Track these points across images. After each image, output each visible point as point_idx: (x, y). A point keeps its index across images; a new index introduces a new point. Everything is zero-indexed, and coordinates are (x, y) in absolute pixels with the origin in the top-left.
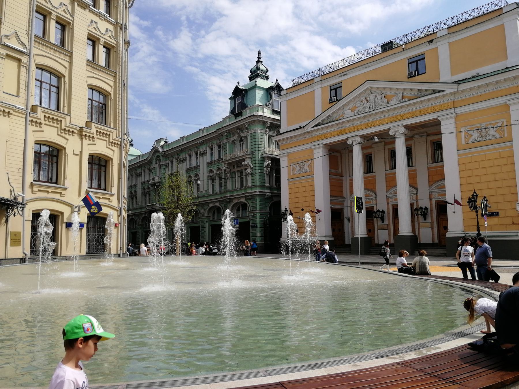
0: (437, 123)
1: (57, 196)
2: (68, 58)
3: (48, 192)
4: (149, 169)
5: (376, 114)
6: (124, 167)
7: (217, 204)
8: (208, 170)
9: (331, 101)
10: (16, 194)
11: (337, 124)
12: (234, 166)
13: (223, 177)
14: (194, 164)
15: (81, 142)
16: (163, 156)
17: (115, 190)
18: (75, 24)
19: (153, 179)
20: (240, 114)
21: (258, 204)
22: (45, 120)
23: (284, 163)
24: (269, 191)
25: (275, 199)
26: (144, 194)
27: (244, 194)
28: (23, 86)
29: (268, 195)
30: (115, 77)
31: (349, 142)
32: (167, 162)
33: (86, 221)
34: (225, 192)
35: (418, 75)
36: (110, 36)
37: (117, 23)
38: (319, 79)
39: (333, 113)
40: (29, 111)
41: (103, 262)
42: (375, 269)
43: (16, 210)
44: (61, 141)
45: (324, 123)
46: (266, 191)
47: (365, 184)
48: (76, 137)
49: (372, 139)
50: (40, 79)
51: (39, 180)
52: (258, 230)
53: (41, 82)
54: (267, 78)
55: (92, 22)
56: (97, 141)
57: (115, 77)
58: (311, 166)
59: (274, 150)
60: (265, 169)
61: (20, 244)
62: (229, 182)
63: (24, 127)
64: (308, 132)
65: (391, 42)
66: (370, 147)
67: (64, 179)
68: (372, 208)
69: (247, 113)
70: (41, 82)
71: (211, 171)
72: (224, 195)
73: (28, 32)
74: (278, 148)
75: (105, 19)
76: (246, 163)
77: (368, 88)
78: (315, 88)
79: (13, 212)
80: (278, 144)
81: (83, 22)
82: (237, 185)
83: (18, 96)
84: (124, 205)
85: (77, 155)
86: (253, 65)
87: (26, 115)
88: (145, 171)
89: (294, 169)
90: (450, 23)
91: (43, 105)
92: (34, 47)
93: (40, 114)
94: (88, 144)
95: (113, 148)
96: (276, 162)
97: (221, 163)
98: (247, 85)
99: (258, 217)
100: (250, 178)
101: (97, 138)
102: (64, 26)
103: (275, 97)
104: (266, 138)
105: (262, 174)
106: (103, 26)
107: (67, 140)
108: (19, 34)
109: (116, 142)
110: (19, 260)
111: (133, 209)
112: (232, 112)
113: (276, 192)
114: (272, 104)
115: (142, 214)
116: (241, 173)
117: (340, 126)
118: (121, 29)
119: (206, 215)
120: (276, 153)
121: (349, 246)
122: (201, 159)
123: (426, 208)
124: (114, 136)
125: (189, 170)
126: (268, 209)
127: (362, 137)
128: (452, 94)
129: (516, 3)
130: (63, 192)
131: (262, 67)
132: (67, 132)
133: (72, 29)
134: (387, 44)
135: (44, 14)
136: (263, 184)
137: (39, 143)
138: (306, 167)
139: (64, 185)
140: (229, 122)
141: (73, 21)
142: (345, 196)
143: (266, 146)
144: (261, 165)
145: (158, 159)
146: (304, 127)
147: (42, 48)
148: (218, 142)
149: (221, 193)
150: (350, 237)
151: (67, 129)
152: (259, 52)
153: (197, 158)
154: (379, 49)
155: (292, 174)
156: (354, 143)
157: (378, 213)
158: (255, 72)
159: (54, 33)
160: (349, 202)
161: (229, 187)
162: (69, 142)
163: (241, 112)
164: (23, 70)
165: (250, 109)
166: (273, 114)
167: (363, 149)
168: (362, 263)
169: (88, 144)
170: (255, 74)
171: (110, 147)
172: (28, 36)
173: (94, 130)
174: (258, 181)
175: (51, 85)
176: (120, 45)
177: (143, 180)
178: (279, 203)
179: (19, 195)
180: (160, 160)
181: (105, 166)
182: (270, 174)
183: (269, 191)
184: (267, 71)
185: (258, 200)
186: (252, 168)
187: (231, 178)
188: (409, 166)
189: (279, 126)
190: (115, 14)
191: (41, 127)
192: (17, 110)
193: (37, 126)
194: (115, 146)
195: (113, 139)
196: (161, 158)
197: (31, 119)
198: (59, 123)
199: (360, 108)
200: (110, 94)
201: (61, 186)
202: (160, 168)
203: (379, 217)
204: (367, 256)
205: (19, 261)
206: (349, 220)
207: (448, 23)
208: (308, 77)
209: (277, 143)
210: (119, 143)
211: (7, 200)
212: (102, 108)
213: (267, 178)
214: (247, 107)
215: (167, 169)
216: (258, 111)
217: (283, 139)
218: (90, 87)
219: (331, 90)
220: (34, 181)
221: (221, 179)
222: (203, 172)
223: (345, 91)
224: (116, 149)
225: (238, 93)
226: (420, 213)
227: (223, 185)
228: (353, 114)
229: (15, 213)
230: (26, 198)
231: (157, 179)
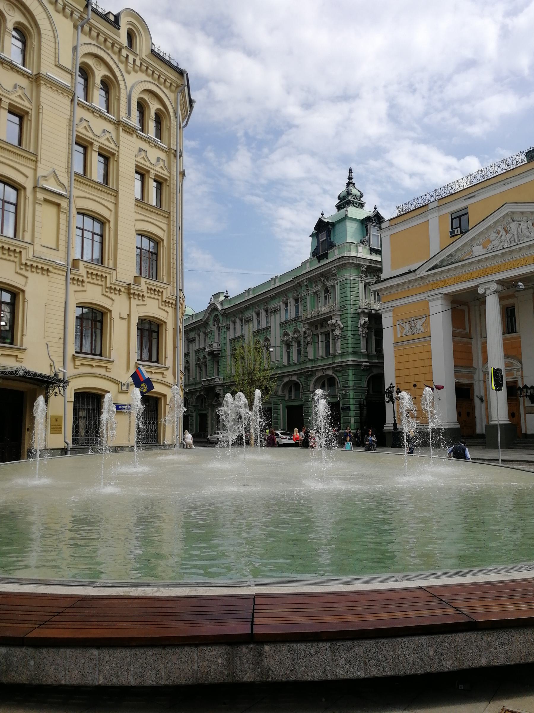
1: (102, 371)
2: (113, 197)
4: (204, 333)
5: (520, 249)
6: (180, 332)
7: (295, 378)
8: (282, 332)
9: (453, 234)
10: (57, 370)
11: (463, 266)
12: (316, 326)
13: (302, 342)
14: (263, 325)
15: (128, 302)
16: (224, 314)
17: (169, 362)
18: (120, 156)
19: (211, 345)
20: (325, 256)
21: (351, 378)
23: (387, 321)
24: (366, 360)
25: (375, 371)
26: (199, 366)
27: (330, 364)
28: (62, 237)
29: (364, 366)
30: (115, 196)
31: (480, 291)
32: (228, 323)
34: (305, 362)
36: (161, 167)
37: (170, 149)
38: (436, 204)
39: (456, 251)
40: (70, 267)
41: (162, 454)
42: (522, 469)
43: (57, 389)
44: (105, 303)
45: (444, 264)
46: (362, 360)
47: (504, 349)
48: (124, 297)
49: (516, 285)
50: (81, 227)
51: (81, 352)
52: (352, 413)
53: (83, 230)
54: (362, 205)
55: (140, 150)
56: (147, 301)
57: (168, 218)
58: (426, 325)
59: (372, 302)
60: (361, 329)
61: (61, 431)
62: (310, 348)
63: (64, 287)
64: (422, 278)
66: (512, 296)
67: (110, 350)
68: (516, 382)
69: (335, 254)
70: (83, 230)
71: (286, 334)
72: (303, 366)
73: (68, 169)
74: (379, 300)
75: (155, 146)
76: (333, 321)
77: (507, 214)
78: (430, 217)
79: (54, 391)
80: (378, 295)
82: (322, 352)
83: (57, 250)
84: (180, 381)
85: (125, 319)
86: (341, 189)
87: (67, 272)
88: (199, 336)
89: (402, 329)
91: (85, 259)
92: (74, 187)
93: (82, 270)
94: (137, 305)
95: (166, 309)
96: (375, 321)
97: (298, 323)
98: (335, 215)
99: (352, 396)
100: (339, 343)
101: (148, 297)
102: (107, 157)
103: (373, 230)
104: (362, 286)
105: (357, 337)
106: (153, 154)
108: (57, 172)
109: (171, 301)
110: (60, 451)
111: (189, 385)
112: (315, 253)
113: (376, 361)
114: (369, 241)
115: (196, 391)
116: (327, 335)
117: (466, 269)
118: (175, 156)
119: (280, 393)
120: (375, 307)
121: (482, 436)
122: (272, 319)
124: (167, 294)
125: (257, 333)
126: (365, 385)
127: (499, 282)
130: (20, 355)
131: (354, 191)
132: (112, 291)
133: (117, 161)
135: (84, 145)
136: (357, 350)
137: (80, 306)
138: (418, 326)
140: (310, 267)
141: (118, 152)
142: (475, 365)
143: (361, 299)
144: (354, 324)
145: (216, 319)
146: (415, 271)
147: (83, 188)
148: (295, 295)
149: (299, 363)
150: (484, 423)
151: (113, 287)
152: (350, 170)
153: (267, 317)
155: (399, 336)
156: (488, 292)
157: (525, 390)
158: (344, 198)
159: (97, 170)
160: (481, 375)
161: (311, 356)
162: (115, 302)
163: (327, 253)
164: (63, 217)
165: (339, 248)
166: (371, 254)
167: (501, 299)
168: (503, 460)
169: (137, 305)
170: (344, 201)
171: (164, 307)
172: (68, 175)
173: (143, 287)
174: (350, 346)
175: (94, 234)
176: (174, 177)
177: (197, 348)
178: (381, 377)
179: (60, 370)
180: (218, 320)
181: (157, 332)
182: (368, 337)
183: (366, 360)
184: (362, 196)
185: (351, 372)
186: (342, 329)
187: (313, 342)
189: (380, 270)
190: (167, 139)
191: (144, 301)
192: (57, 266)
194: (169, 307)
195: (167, 298)
196: (221, 318)
197: (72, 276)
198: (17, 255)
199: (496, 243)
200: (163, 240)
201: (107, 359)
202: (219, 331)
203: (526, 396)
204: (510, 451)
205: (59, 452)
206: (481, 399)
208: (421, 203)
209: (377, 294)
210: (174, 302)
211: (48, 377)
212: (152, 257)
213: (363, 342)
214: (335, 246)
215: (228, 333)
216: (349, 251)
217: (386, 288)
218: (139, 232)
219: (452, 219)
220: (76, 352)
221: (298, 344)
222: (276, 336)
223: (473, 220)
224: (170, 310)
225: (323, 228)
227: (302, 352)
228: (484, 251)
229: (56, 393)
230: (67, 375)
231: (215, 346)
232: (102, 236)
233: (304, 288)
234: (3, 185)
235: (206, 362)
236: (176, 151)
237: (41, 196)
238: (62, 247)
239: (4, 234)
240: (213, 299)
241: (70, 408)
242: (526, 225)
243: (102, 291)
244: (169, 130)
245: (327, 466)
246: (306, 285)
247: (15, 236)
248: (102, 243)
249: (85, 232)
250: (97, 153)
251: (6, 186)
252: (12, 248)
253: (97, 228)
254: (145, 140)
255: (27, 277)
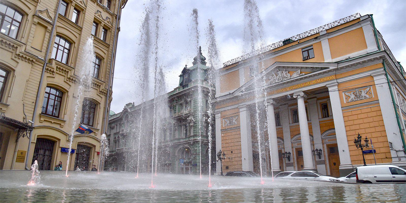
0: (325, 91)
1: (58, 127)
3: (51, 122)
22: (57, 70)
27: (188, 141)
33: (76, 148)
35: (309, 59)
43: (25, 133)
44: (65, 86)
50: (58, 43)
53: (58, 45)
55: (98, 11)
58: (238, 120)
61: (24, 161)
63: (41, 73)
65: (289, 39)
70: (58, 45)
75: (106, 11)
76: (190, 118)
81: (91, 10)
88: (117, 125)
90: (327, 28)
92: (57, 21)
95: (101, 96)
100: (192, 130)
106: (105, 15)
107: (70, 86)
109: (104, 92)
112: (181, 84)
123: (320, 150)
128: (334, 70)
129: (368, 15)
130: (62, 124)
134: (287, 40)
138: (234, 121)
139: (64, 119)
141: (85, 9)
154: (282, 43)
157: (286, 154)
175: (64, 48)
188: (308, 120)
192: (38, 60)
193: (51, 74)
195: (102, 89)
197: (47, 68)
207: (325, 28)
210: (106, 92)
211: (19, 123)
224: (103, 97)
225: (185, 71)
226: (316, 153)
232: (69, 50)
233: (175, 101)
234: (14, 11)
235: (119, 139)
236: (117, 15)
237: (36, 20)
238: (44, 50)
239: (10, 36)
240: (126, 106)
241: (33, 147)
242: (285, 72)
243: (65, 79)
244: (115, 5)
245: (256, 22)
246: (176, 100)
247: (16, 38)
248: (69, 54)
249: (60, 46)
250: (74, 7)
251: (16, 13)
252: (12, 44)
253: (67, 46)
254: (101, 7)
255: (18, 63)
